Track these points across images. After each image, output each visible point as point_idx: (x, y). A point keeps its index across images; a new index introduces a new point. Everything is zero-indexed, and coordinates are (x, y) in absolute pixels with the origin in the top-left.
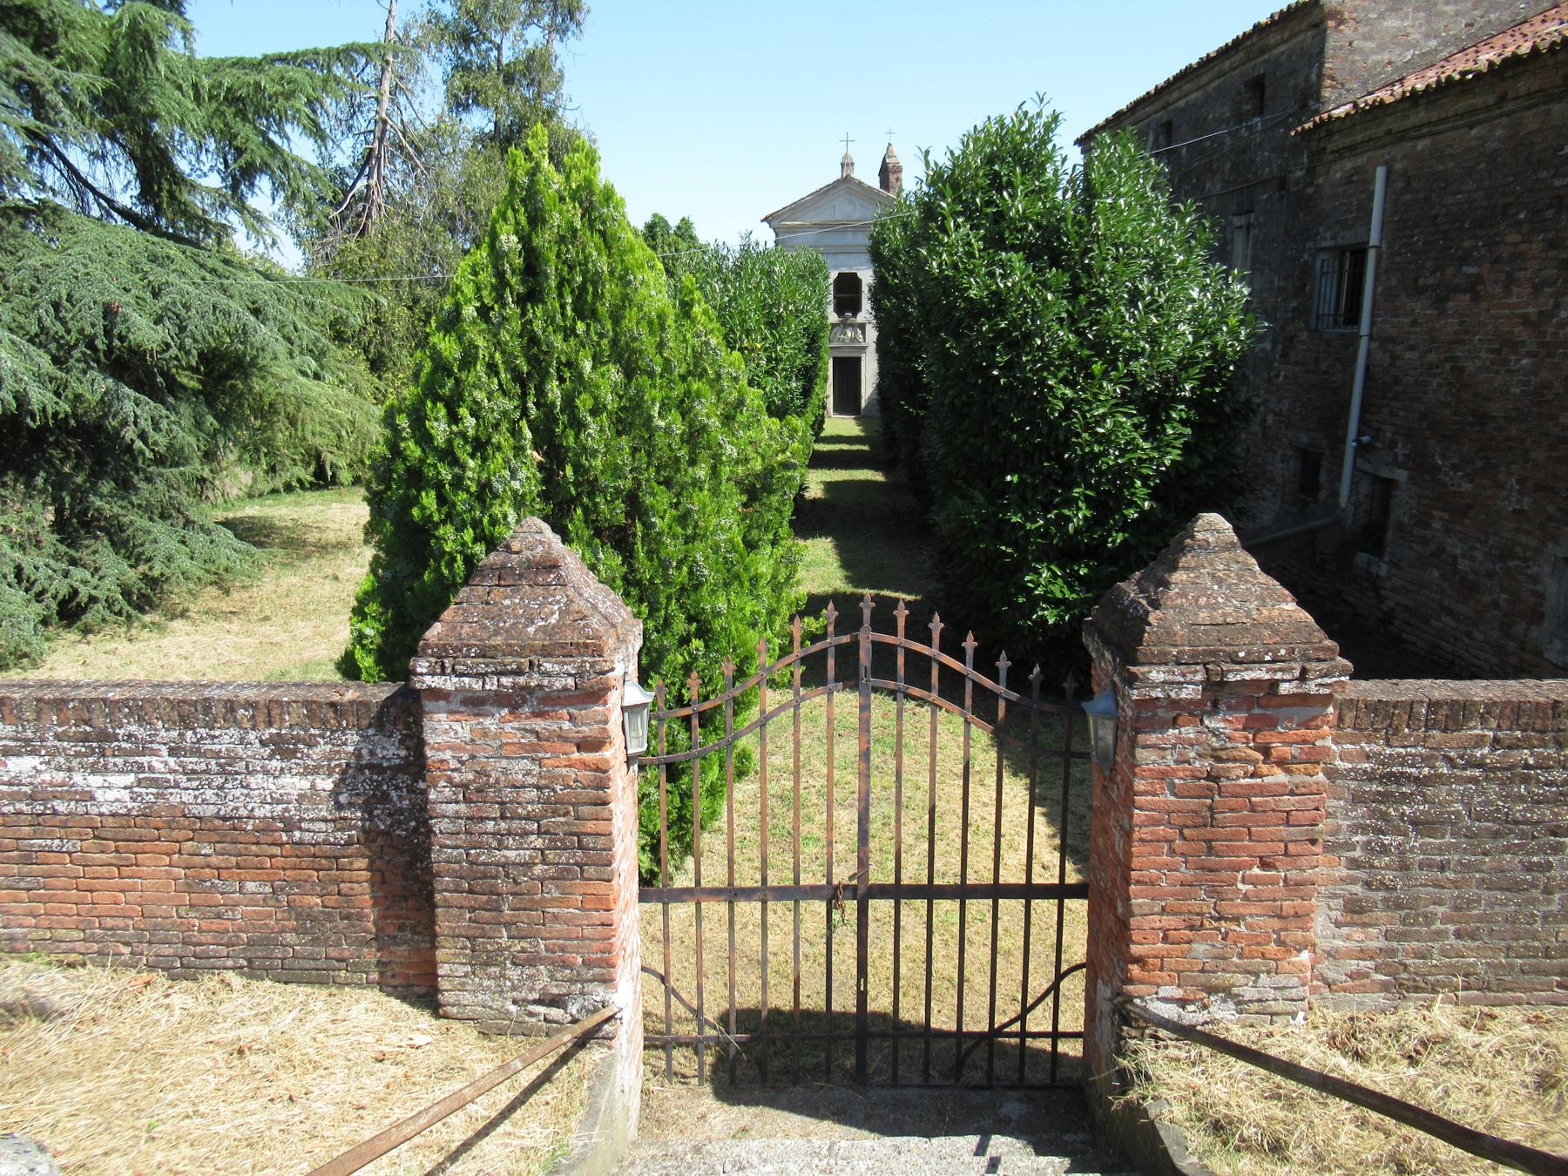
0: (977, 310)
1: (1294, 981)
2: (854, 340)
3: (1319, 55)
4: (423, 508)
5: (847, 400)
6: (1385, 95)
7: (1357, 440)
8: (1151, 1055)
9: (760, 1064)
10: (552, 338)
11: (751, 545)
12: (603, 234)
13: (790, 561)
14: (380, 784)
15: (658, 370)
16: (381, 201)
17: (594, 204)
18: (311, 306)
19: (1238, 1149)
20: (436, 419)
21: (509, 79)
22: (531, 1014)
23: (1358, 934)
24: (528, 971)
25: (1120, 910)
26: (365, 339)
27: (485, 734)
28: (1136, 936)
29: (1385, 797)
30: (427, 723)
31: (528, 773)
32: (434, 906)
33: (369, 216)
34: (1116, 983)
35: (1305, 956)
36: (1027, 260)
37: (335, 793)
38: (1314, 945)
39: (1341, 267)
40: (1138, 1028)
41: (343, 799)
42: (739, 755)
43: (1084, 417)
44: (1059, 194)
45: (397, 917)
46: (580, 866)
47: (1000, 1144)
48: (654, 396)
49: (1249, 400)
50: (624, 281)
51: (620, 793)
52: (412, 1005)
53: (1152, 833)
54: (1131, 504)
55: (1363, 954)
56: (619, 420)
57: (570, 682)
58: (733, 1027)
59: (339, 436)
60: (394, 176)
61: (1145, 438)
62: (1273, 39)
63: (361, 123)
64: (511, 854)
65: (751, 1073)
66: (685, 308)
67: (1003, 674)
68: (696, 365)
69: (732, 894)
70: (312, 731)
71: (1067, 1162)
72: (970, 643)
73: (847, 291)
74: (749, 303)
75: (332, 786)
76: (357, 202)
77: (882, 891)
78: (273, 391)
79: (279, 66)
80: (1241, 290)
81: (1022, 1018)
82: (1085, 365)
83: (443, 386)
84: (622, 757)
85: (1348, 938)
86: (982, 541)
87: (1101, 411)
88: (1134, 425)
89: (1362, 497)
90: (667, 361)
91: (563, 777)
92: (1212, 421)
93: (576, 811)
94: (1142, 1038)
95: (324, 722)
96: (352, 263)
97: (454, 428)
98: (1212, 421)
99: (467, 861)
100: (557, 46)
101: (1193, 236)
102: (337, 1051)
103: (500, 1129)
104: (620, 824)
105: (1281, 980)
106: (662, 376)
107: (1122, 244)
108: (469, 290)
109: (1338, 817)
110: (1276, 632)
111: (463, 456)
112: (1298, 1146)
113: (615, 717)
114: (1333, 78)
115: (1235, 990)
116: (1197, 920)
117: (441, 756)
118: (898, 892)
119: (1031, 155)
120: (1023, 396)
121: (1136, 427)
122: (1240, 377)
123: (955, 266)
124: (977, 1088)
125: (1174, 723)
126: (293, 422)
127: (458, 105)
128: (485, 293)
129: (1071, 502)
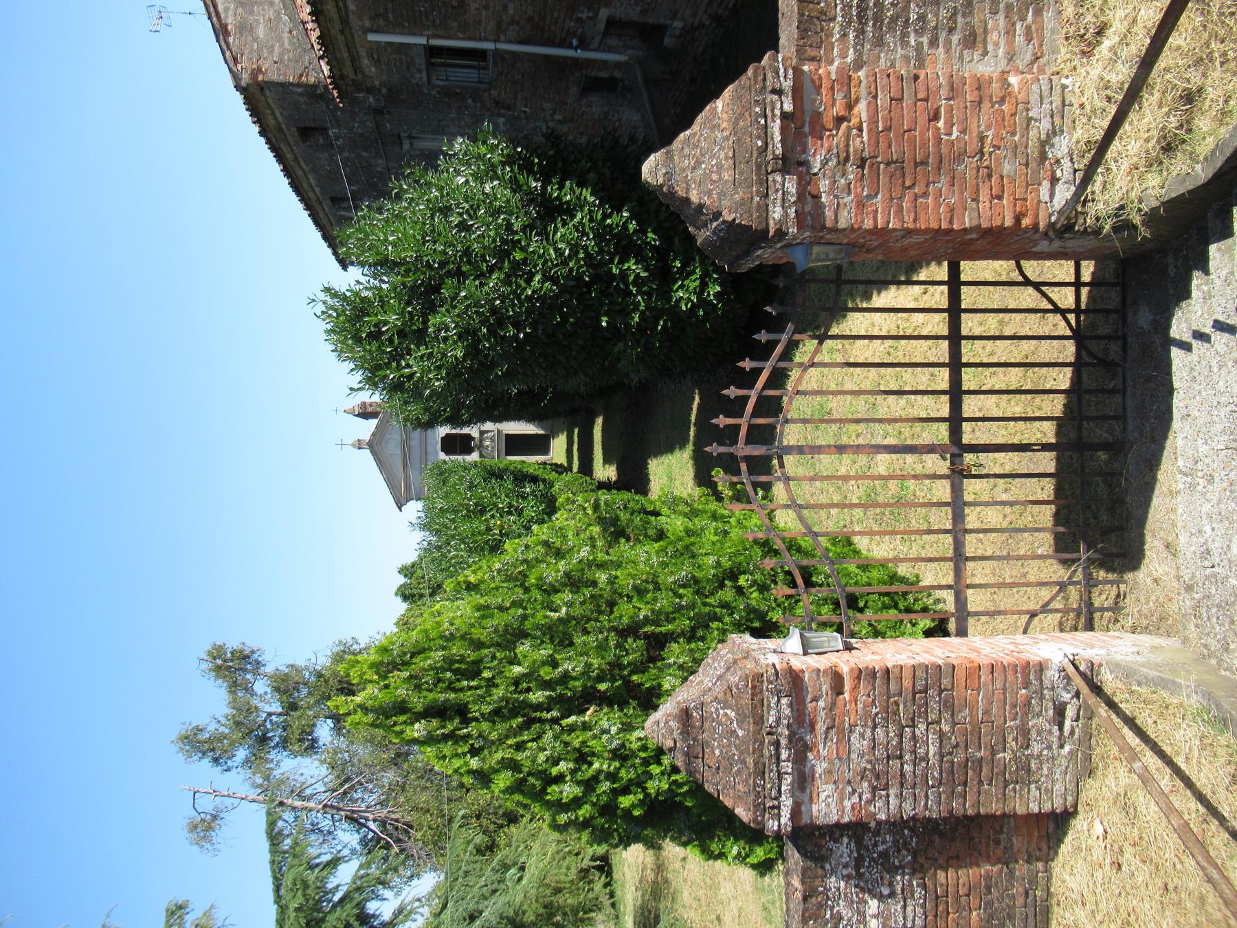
0: (473, 351)
1: (1035, 88)
2: (492, 439)
3: (283, 86)
4: (633, 806)
5: (539, 445)
6: (314, 36)
7: (576, 49)
8: (1101, 206)
9: (1106, 532)
10: (495, 697)
11: (661, 535)
12: (413, 655)
13: (674, 502)
14: (872, 859)
15: (520, 611)
16: (385, 811)
17: (390, 662)
18: (467, 873)
19: (1189, 131)
20: (561, 792)
21: (293, 707)
22: (1072, 733)
23: (994, 36)
24: (1033, 735)
25: (974, 236)
26: (492, 827)
27: (829, 772)
28: (997, 222)
29: (878, 19)
30: (821, 821)
31: (862, 736)
32: (978, 815)
33: (397, 820)
34: (1037, 236)
35: (1013, 80)
37: (881, 898)
38: (1003, 72)
39: (442, 65)
40: (1076, 217)
41: (886, 891)
42: (833, 544)
43: (557, 265)
44: (385, 286)
45: (988, 846)
46: (941, 691)
47: (1179, 328)
48: (543, 616)
49: (544, 135)
51: (878, 658)
52: (1065, 834)
53: (908, 212)
54: (625, 227)
55: (1010, 32)
56: (561, 643)
57: (784, 701)
58: (1074, 556)
59: (570, 852)
60: (366, 799)
61: (573, 217)
62: (271, 122)
63: (326, 824)
64: (932, 750)
65: (1114, 539)
66: (471, 587)
67: (772, 337)
68: (517, 579)
69: (959, 558)
70: (828, 916)
71: (1196, 274)
72: (747, 364)
73: (455, 445)
75: (875, 901)
76: (386, 830)
77: (956, 433)
78: (534, 905)
79: (282, 892)
80: (459, 144)
81: (1063, 312)
82: (516, 265)
83: (534, 786)
84: (846, 655)
85: (997, 45)
86: (653, 344)
87: (552, 252)
88: (563, 226)
89: (621, 44)
90: (514, 604)
91: (865, 706)
92: (560, 165)
93: (895, 695)
94: (1085, 214)
95: (820, 906)
96: (433, 836)
97: (568, 778)
98: (560, 165)
99: (938, 787)
100: (269, 669)
101: (417, 182)
102: (1112, 905)
103: (1183, 766)
104: (904, 657)
105: (1034, 98)
106: (525, 609)
107: (423, 238)
108: (457, 763)
109: (894, 57)
110: (742, 115)
111: (591, 772)
112: (1188, 80)
113: (813, 661)
114: (301, 75)
115: (1043, 137)
116: (983, 172)
117: (848, 809)
118: (955, 420)
119: (354, 308)
120: (540, 314)
121: (564, 224)
122: (527, 142)
123: (439, 368)
124: (1125, 348)
125: (816, 197)
126: (558, 891)
127: (312, 747)
128: (460, 750)
129: (624, 275)
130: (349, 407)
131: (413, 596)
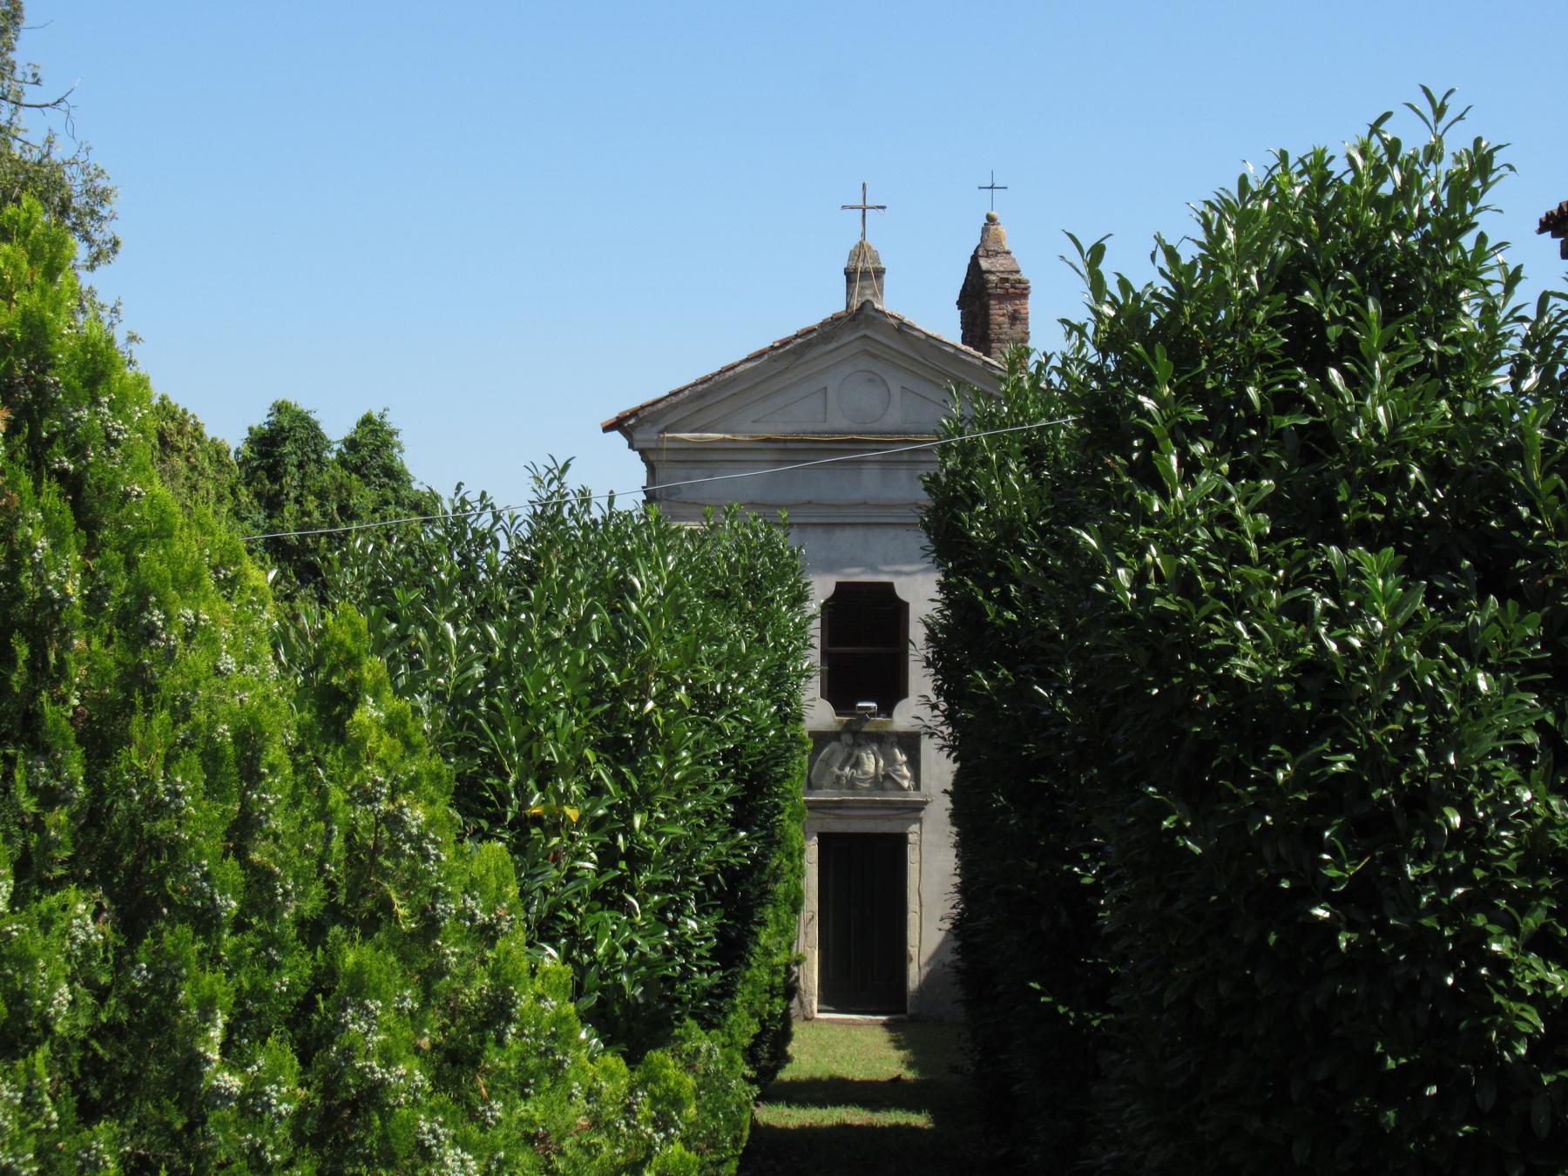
0: (1255, 719)
2: (885, 780)
5: (864, 966)
12: (72, 485)
36: (1409, 570)
44: (1501, 379)
50: (133, 628)
56: (93, 1067)
66: (331, 706)
73: (864, 638)
74: (552, 683)
90: (260, 879)
106: (240, 926)
119: (1411, 263)
130: (1010, 236)
131: (275, 474)
